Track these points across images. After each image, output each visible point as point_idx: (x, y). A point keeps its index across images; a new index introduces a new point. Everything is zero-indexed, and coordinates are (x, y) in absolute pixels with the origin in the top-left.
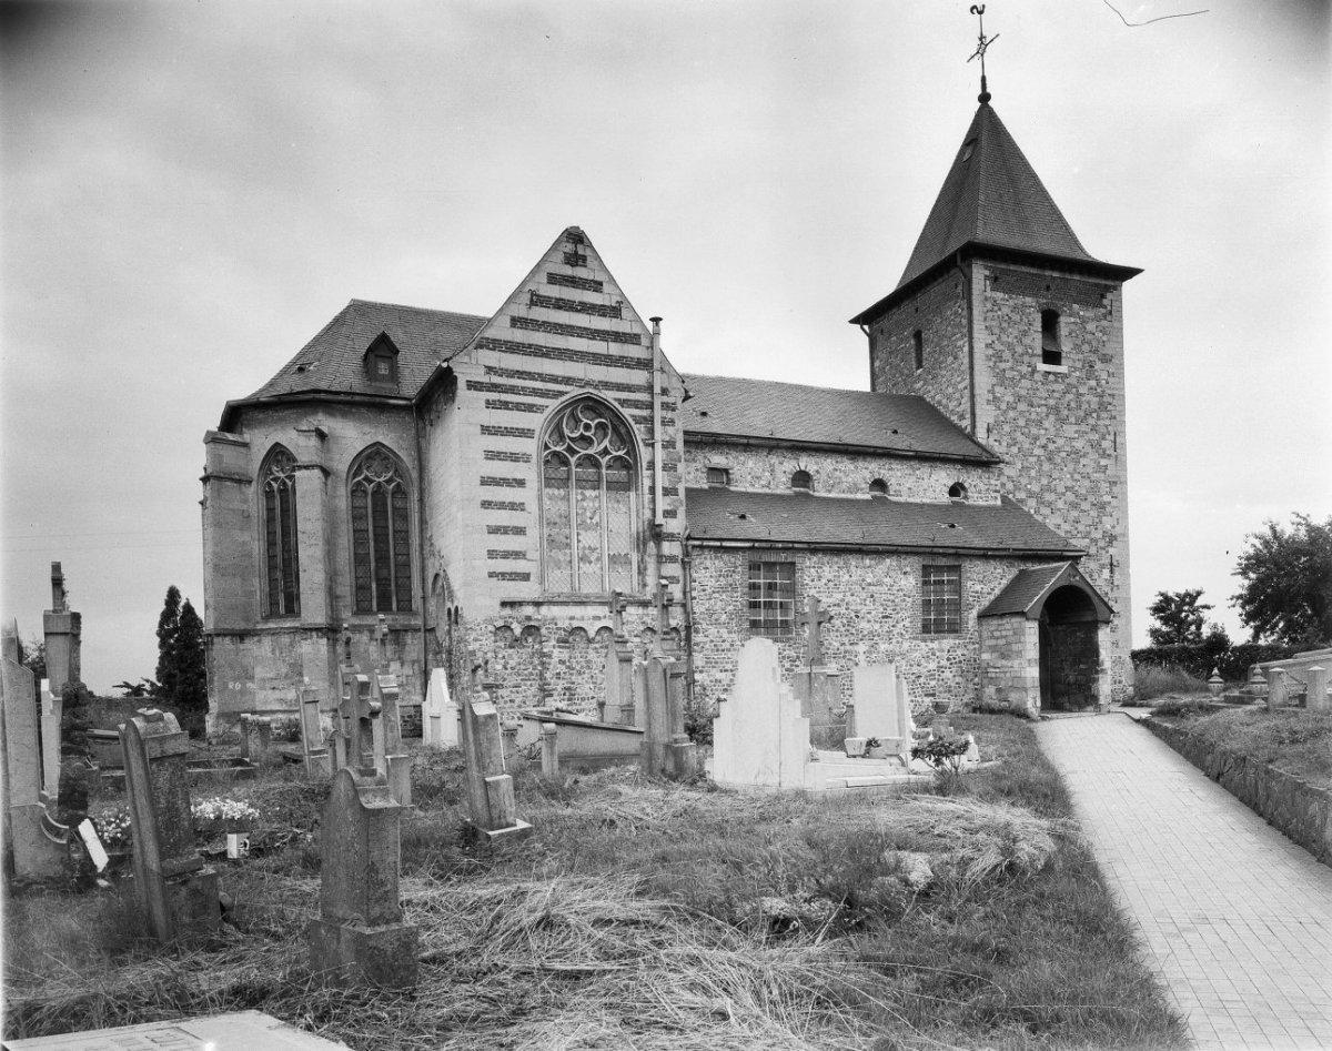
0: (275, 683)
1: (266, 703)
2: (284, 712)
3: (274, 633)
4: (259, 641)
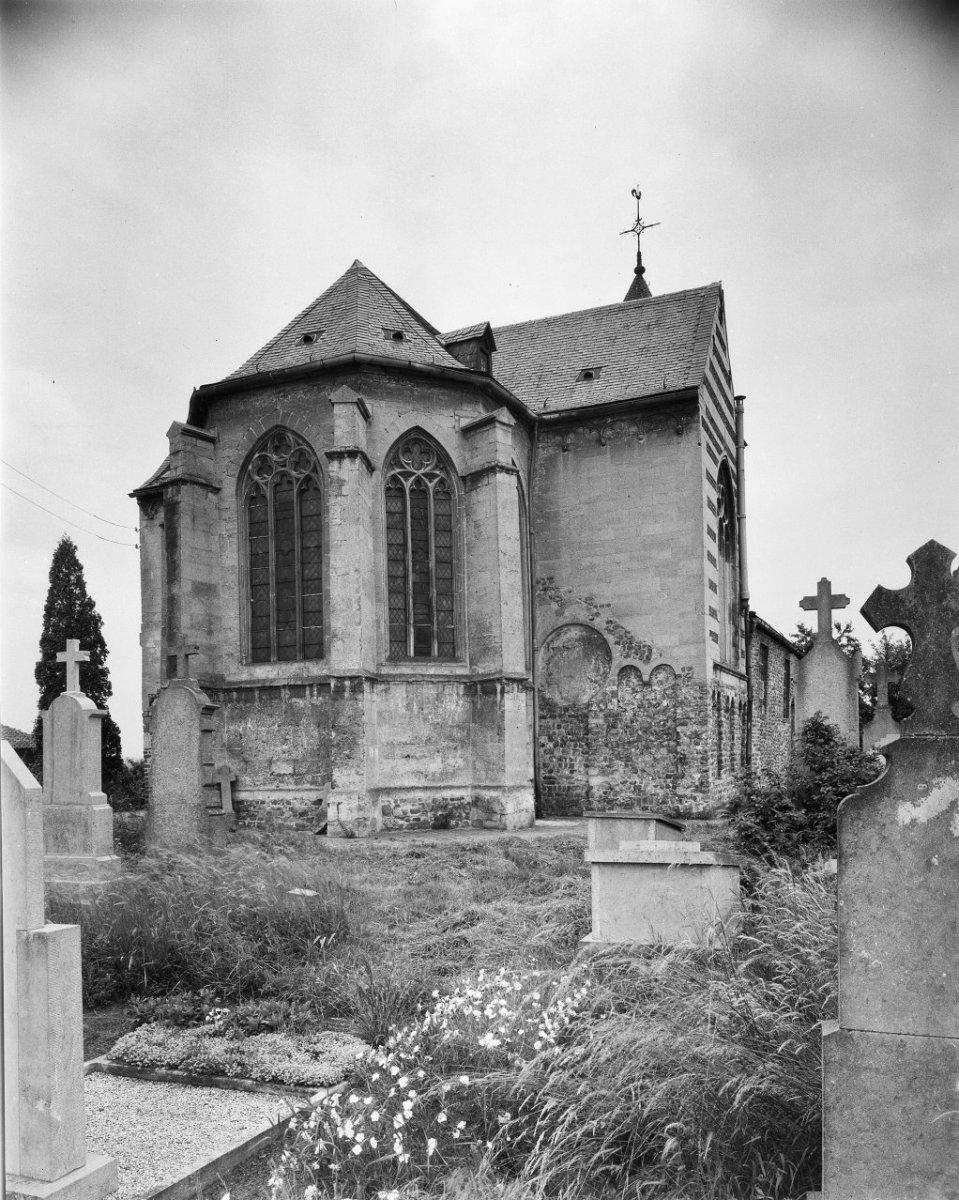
0: (410, 750)
1: (393, 776)
2: (426, 788)
3: (409, 681)
4: (386, 691)
